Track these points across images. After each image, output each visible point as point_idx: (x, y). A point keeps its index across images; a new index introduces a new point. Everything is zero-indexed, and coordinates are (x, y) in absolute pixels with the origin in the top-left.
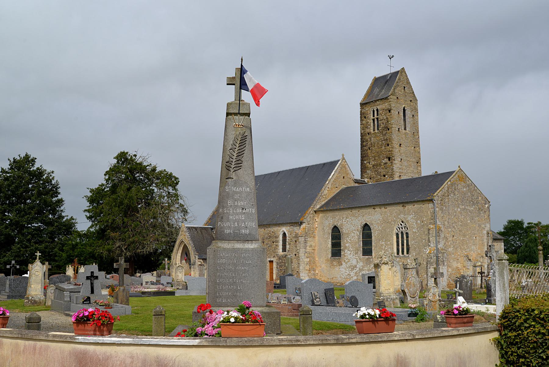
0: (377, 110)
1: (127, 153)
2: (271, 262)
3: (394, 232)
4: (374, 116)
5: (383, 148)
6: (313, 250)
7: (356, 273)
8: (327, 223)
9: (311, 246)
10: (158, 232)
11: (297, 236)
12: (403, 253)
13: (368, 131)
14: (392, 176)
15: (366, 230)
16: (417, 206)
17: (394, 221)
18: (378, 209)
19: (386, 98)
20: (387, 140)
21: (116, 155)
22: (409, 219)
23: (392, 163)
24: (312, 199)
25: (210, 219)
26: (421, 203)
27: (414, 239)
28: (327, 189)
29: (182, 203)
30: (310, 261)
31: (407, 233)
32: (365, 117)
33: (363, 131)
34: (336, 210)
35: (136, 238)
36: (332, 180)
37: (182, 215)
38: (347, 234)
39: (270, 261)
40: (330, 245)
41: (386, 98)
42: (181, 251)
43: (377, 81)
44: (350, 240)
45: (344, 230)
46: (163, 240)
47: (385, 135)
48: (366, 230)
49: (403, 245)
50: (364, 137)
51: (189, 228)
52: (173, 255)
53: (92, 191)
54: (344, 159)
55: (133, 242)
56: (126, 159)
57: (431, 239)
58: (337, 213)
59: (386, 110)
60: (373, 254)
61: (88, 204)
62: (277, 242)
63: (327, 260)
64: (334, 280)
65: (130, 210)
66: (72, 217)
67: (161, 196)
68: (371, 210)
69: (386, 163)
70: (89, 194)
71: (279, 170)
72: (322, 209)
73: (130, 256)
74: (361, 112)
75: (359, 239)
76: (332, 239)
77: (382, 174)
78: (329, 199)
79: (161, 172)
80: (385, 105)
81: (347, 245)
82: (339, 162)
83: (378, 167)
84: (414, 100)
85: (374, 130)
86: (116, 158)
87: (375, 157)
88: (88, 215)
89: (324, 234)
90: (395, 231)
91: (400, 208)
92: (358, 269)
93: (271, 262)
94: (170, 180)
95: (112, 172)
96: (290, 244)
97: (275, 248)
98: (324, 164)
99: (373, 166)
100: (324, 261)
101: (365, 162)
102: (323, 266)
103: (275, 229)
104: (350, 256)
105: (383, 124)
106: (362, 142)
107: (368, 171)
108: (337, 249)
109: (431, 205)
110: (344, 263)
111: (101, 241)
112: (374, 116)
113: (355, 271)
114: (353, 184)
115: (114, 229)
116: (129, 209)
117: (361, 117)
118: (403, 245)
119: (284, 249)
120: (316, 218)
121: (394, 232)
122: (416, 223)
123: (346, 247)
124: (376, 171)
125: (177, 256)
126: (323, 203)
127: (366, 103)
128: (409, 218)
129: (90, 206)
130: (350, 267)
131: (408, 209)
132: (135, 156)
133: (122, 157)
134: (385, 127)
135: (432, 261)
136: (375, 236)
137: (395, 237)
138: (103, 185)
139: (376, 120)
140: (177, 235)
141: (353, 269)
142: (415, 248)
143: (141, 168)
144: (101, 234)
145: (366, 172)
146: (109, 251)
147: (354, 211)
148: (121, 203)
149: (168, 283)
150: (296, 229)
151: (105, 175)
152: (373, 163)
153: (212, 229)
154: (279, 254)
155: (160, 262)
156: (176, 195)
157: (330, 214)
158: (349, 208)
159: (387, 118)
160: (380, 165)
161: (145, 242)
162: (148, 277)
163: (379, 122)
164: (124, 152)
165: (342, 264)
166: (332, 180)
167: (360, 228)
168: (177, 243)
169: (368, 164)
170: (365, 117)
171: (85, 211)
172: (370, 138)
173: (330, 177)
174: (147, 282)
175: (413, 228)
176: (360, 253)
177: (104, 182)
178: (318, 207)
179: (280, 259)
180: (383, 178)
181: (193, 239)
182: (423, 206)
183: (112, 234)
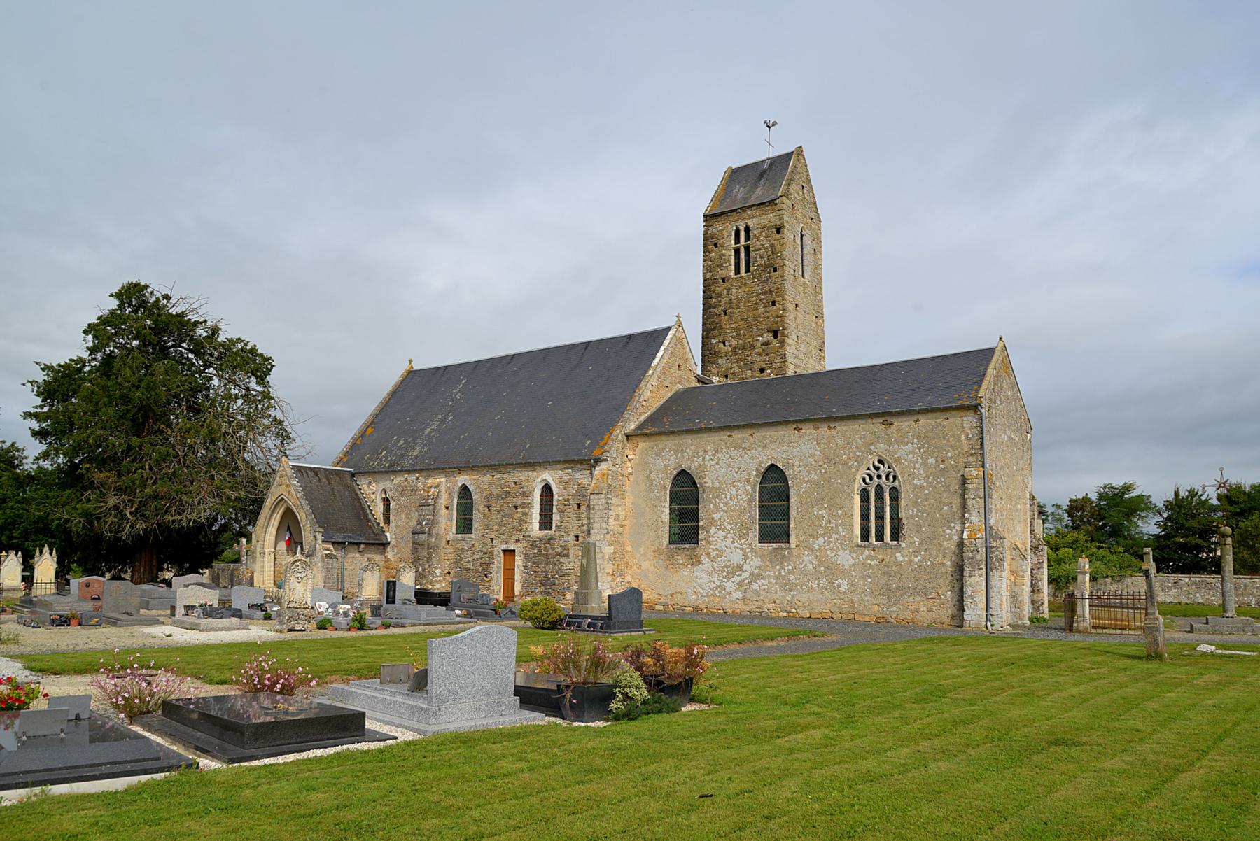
0: (747, 229)
1: (146, 287)
2: (509, 553)
3: (857, 485)
4: (737, 241)
5: (761, 309)
6: (622, 526)
7: (741, 584)
8: (659, 463)
9: (617, 518)
10: (220, 476)
11: (581, 492)
12: (880, 537)
13: (722, 273)
14: (783, 368)
16: (925, 421)
17: (857, 459)
19: (772, 202)
20: (771, 292)
21: (115, 290)
23: (783, 341)
24: (619, 409)
25: (346, 454)
26: (938, 414)
27: (915, 504)
28: (649, 386)
29: (280, 417)
30: (615, 553)
31: (894, 490)
32: (716, 245)
33: (709, 275)
34: (688, 432)
35: (162, 488)
36: (659, 369)
37: (278, 442)
38: (717, 489)
39: (505, 551)
40: (666, 516)
41: (772, 202)
42: (276, 524)
43: (735, 176)
44: (726, 504)
46: (233, 495)
47: (766, 281)
49: (880, 518)
50: (712, 288)
51: (299, 470)
52: (256, 532)
53: (47, 368)
54: (680, 325)
55: (155, 497)
56: (143, 304)
57: (970, 503)
58: (688, 439)
59: (769, 228)
60: (793, 539)
61: (38, 401)
62: (529, 506)
63: (658, 551)
64: (678, 600)
65: (145, 419)
66: (13, 444)
67: (230, 398)
69: (767, 343)
70: (41, 377)
71: (513, 352)
72: (645, 431)
73: (145, 530)
74: (706, 233)
75: (751, 501)
76: (672, 501)
77: (757, 367)
78: (653, 409)
79: (232, 342)
80: (770, 218)
82: (672, 332)
83: (747, 352)
84: (816, 219)
85: (738, 271)
86: (118, 295)
87: (738, 329)
88: (35, 425)
89: (651, 490)
91: (876, 426)
92: (746, 575)
93: (509, 553)
94: (253, 364)
95: (100, 330)
96: (561, 512)
97: (521, 520)
98: (630, 337)
99: (735, 349)
100: (650, 554)
101: (714, 341)
102: (646, 565)
103: (522, 475)
104: (723, 544)
105: (761, 257)
106: (707, 295)
107: (720, 361)
108: (686, 523)
109: (969, 420)
110: (705, 560)
111: (68, 492)
112: (737, 241)
113: (737, 579)
114: (695, 384)
115: (103, 463)
116: (146, 418)
117: (705, 246)
118: (880, 518)
119: (546, 523)
120: (628, 452)
121: (857, 485)
122: (925, 464)
123: (712, 522)
124: (741, 360)
125: (267, 532)
126: (642, 418)
127: (720, 215)
128: (903, 451)
129: (42, 407)
130: (722, 569)
131: (899, 430)
132: (167, 297)
133: (132, 294)
134: (766, 266)
135: (978, 557)
137: (857, 498)
138: (81, 361)
139: (742, 250)
140: (268, 487)
141: (732, 574)
142: (919, 526)
143: (182, 326)
144: (71, 478)
145: (715, 362)
146: (88, 516)
147: (738, 435)
148: (125, 399)
149: (252, 606)
150: (581, 477)
151: (85, 332)
152: (734, 343)
153: (353, 475)
154: (533, 534)
155: (222, 547)
156: (267, 396)
157: (669, 443)
159: (772, 246)
160: (752, 346)
161: (185, 498)
162: (191, 590)
163: (752, 254)
164: (137, 285)
165: (699, 562)
166: (659, 369)
167: (755, 476)
168: (268, 504)
169: (721, 345)
170: (716, 245)
171: (27, 415)
172: (728, 290)
173: (656, 361)
174: (189, 609)
175: (914, 476)
176: (754, 535)
177: (86, 355)
178: (633, 426)
179: (533, 545)
180: (758, 374)
181: (308, 494)
182: (946, 422)
183: (99, 476)
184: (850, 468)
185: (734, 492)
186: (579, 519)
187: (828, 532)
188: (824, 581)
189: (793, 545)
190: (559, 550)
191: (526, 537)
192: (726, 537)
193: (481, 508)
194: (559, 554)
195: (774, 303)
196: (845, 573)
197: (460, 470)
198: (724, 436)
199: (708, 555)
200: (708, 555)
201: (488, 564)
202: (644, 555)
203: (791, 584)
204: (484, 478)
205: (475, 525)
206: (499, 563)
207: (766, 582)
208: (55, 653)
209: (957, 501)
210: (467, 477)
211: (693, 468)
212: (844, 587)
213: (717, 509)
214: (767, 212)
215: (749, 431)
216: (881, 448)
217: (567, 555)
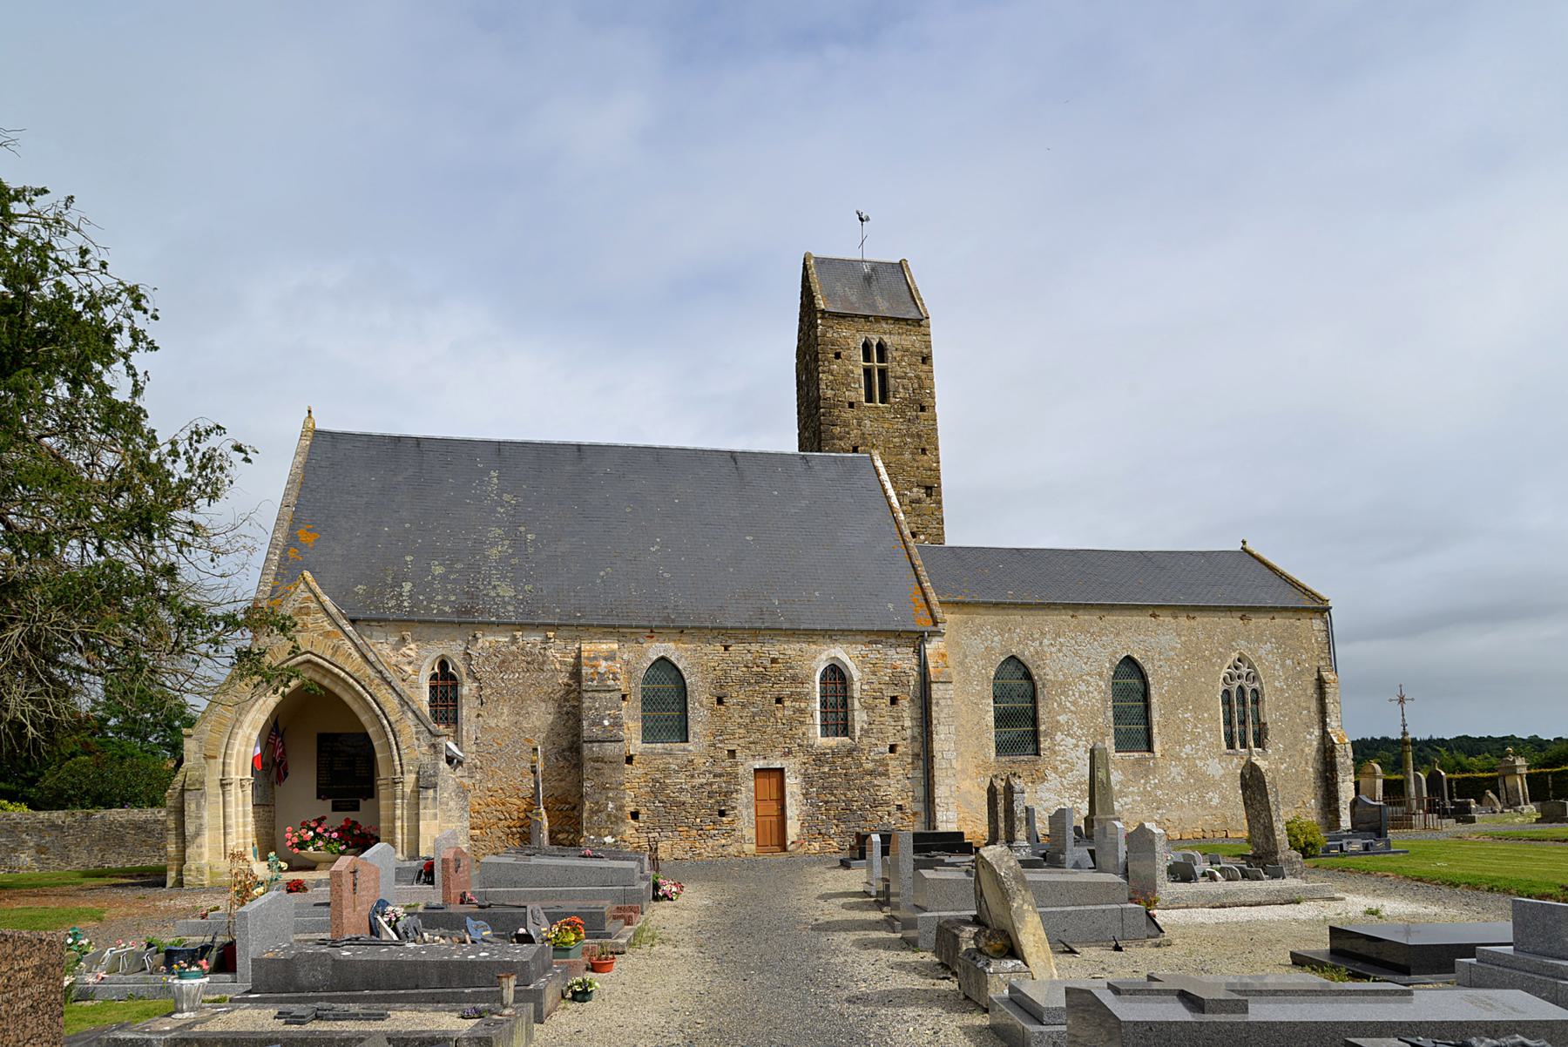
5: (907, 456)
8: (977, 644)
15: (1131, 680)
18: (1166, 619)
22: (1262, 652)
27: (1278, 708)
32: (838, 356)
40: (990, 719)
44: (1074, 703)
45: (1049, 671)
48: (1131, 680)
58: (1016, 617)
60: (1157, 747)
68: (1143, 619)
69: (918, 501)
81: (1062, 719)
85: (870, 399)
90: (1221, 687)
96: (869, 708)
97: (790, 720)
100: (972, 770)
103: (791, 649)
109: (1317, 624)
110: (1052, 776)
122: (1283, 666)
123: (1057, 726)
131: (1257, 627)
136: (1161, 695)
142: (1282, 730)
147: (1084, 617)
158: (1066, 606)
184: (1214, 665)
185: (1083, 688)
186: (897, 719)
187: (1196, 738)
188: (1194, 796)
189: (1158, 755)
190: (870, 766)
191: (806, 749)
192: (1076, 746)
193: (704, 698)
194: (871, 773)
195: (924, 450)
196: (1216, 785)
197: (653, 632)
198: (1065, 617)
199: (1055, 769)
200: (1055, 769)
201: (728, 794)
202: (963, 771)
203: (1160, 801)
204: (709, 649)
205: (694, 728)
206: (745, 795)
207: (1129, 800)
208: (1148, 1001)
209: (1314, 705)
210: (671, 645)
211: (1027, 653)
212: (1215, 801)
213: (1064, 709)
214: (908, 333)
215: (1098, 613)
216: (1242, 646)
217: (885, 774)
